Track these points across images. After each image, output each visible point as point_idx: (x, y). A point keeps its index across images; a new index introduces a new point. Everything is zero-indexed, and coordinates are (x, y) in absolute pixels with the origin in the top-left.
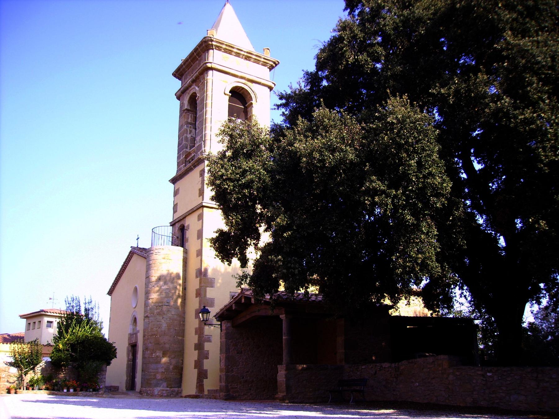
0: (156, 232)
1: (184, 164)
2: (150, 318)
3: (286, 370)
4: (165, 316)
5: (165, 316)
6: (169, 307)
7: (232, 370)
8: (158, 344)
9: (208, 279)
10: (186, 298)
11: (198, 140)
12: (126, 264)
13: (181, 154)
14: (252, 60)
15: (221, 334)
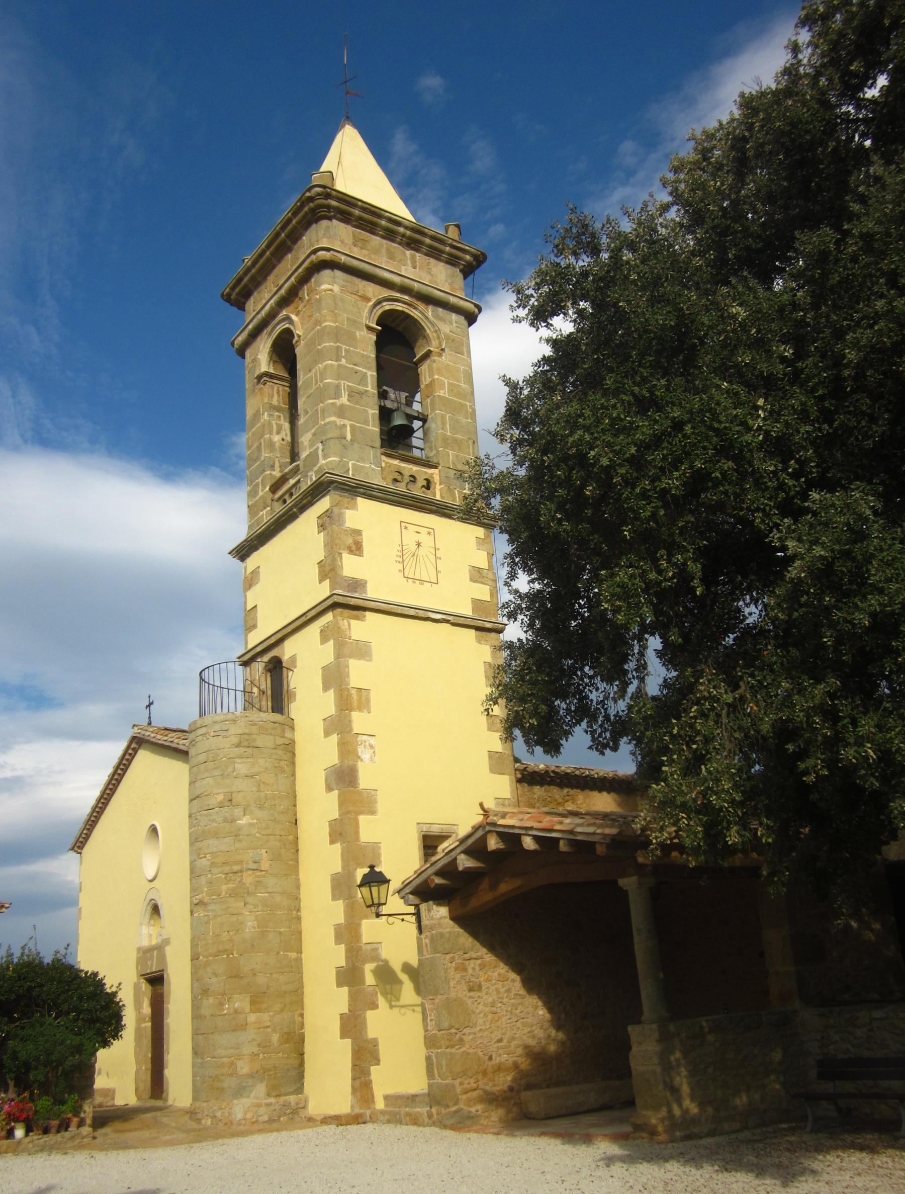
0: (211, 682)
1: (269, 508)
2: (210, 907)
3: (659, 1041)
4: (250, 899)
5: (250, 899)
6: (259, 873)
7: (461, 1040)
8: (236, 976)
9: (360, 793)
10: (300, 847)
11: (306, 443)
12: (122, 769)
13: (257, 485)
14: (424, 249)
15: (419, 941)
